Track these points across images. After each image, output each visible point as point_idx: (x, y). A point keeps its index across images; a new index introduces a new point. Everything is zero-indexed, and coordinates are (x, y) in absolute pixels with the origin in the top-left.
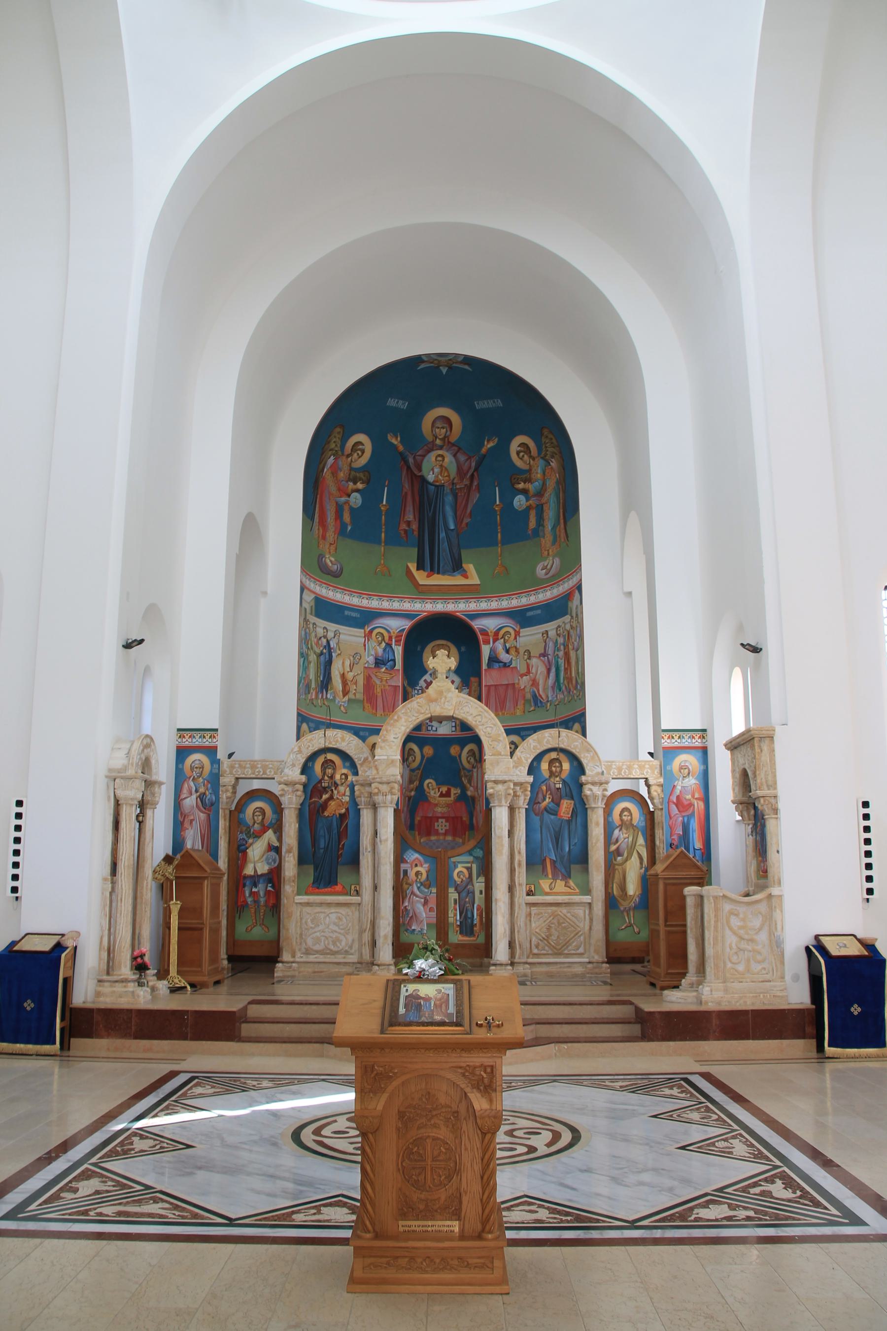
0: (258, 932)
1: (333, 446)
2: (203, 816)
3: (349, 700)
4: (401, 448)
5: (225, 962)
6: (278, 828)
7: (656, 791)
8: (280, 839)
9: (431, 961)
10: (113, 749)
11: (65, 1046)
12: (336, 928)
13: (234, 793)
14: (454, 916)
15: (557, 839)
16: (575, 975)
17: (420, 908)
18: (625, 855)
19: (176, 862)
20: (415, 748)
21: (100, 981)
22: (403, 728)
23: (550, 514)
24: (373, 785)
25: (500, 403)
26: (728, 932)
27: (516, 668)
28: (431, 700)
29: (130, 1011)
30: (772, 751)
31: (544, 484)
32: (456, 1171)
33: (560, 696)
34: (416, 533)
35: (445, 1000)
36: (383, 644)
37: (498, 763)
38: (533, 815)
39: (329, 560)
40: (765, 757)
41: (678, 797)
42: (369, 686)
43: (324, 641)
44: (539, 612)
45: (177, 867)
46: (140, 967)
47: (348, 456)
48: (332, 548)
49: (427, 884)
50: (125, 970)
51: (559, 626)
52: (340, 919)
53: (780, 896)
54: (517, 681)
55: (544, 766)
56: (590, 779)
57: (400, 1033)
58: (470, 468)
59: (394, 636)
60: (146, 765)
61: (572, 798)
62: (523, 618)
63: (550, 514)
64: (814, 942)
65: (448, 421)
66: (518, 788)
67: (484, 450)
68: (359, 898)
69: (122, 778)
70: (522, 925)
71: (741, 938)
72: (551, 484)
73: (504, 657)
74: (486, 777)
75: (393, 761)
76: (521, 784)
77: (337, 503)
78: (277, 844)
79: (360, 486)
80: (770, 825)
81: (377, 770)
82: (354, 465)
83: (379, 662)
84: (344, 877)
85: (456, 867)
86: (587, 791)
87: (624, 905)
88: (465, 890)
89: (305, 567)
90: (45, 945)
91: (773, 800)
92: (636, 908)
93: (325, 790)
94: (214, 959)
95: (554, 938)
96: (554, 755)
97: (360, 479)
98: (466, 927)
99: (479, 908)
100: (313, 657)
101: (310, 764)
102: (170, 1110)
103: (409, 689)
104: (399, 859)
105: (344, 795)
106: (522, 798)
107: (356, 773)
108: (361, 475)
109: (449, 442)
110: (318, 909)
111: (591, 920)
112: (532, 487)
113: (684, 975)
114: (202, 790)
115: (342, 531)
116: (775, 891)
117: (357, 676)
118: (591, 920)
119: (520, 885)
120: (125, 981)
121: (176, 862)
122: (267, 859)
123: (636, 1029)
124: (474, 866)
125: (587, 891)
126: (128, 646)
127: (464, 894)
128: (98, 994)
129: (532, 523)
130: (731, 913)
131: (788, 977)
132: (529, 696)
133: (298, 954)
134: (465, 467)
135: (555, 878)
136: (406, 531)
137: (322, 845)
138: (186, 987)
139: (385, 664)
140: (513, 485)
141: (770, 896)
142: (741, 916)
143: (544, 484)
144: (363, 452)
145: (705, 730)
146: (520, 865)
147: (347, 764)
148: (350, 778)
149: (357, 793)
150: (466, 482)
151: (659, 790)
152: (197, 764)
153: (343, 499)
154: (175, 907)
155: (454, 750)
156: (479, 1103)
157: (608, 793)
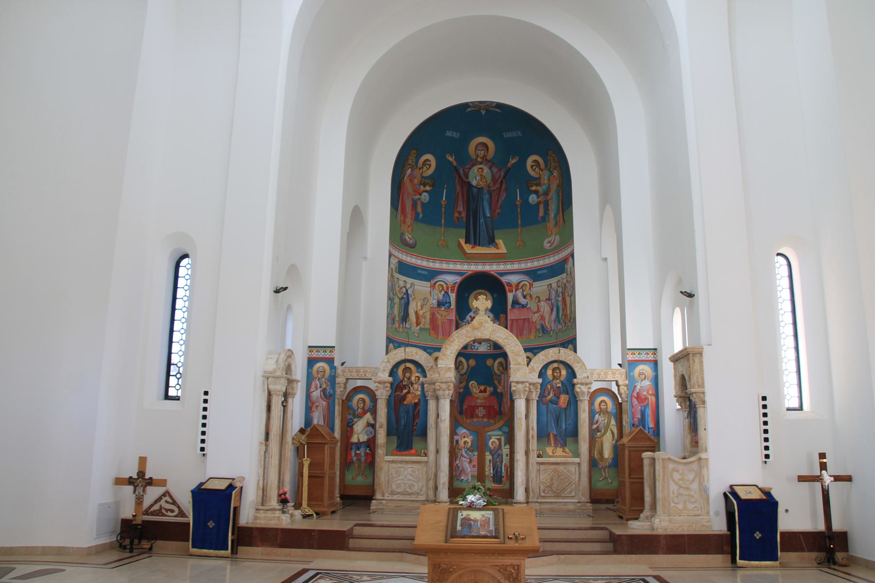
0: (360, 480)
1: (410, 162)
3: (421, 329)
4: (455, 164)
5: (338, 499)
6: (374, 412)
7: (623, 389)
8: (375, 419)
11: (234, 551)
13: (345, 388)
14: (489, 471)
15: (558, 421)
16: (569, 511)
17: (466, 465)
21: (257, 510)
25: (520, 134)
26: (672, 483)
28: (475, 329)
29: (277, 529)
30: (701, 362)
31: (549, 187)
34: (465, 219)
39: (408, 237)
40: (696, 366)
42: (433, 319)
43: (404, 289)
45: (308, 436)
46: (284, 501)
49: (471, 450)
50: (274, 503)
52: (414, 472)
55: (549, 372)
56: (579, 381)
57: (457, 542)
60: (288, 369)
61: (568, 394)
62: (535, 275)
63: (553, 207)
64: (729, 490)
67: (509, 165)
71: (681, 487)
72: (554, 187)
73: (522, 301)
74: (511, 379)
75: (449, 368)
76: (534, 384)
79: (428, 188)
80: (700, 412)
83: (440, 304)
84: (417, 445)
85: (490, 438)
86: (577, 389)
87: (602, 464)
88: (496, 453)
89: (392, 242)
90: (222, 485)
91: (701, 395)
92: (609, 466)
93: (405, 387)
95: (555, 486)
96: (555, 365)
98: (497, 478)
100: (397, 300)
103: (460, 322)
104: (453, 433)
106: (534, 393)
107: (425, 376)
108: (429, 181)
110: (400, 465)
111: (580, 474)
112: (540, 189)
113: (642, 511)
114: (324, 386)
115: (416, 218)
117: (426, 313)
118: (580, 474)
123: (610, 546)
124: (503, 438)
125: (577, 454)
127: (496, 456)
128: (256, 518)
129: (541, 213)
130: (674, 470)
131: (712, 513)
132: (538, 327)
133: (386, 495)
134: (497, 177)
135: (556, 446)
136: (458, 218)
137: (403, 423)
140: (528, 188)
141: (700, 459)
143: (549, 187)
144: (430, 166)
148: (421, 379)
149: (426, 389)
150: (498, 186)
151: (625, 388)
154: (306, 462)
155: (489, 362)
157: (592, 391)
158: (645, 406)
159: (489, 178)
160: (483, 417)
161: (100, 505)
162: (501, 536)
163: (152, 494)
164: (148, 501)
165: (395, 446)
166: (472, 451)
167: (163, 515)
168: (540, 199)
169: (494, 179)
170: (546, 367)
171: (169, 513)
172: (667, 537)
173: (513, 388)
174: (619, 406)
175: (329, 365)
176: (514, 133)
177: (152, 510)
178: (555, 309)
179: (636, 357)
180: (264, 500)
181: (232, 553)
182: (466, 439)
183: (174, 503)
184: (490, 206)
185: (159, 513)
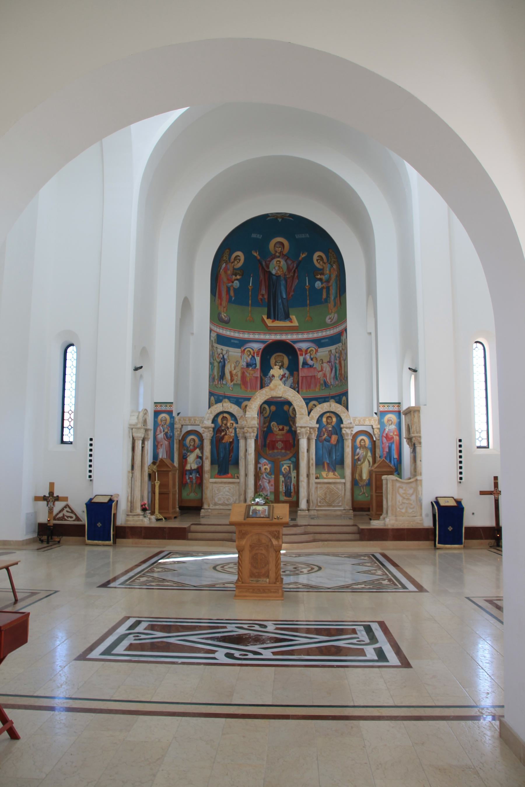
0: (192, 496)
1: (225, 258)
2: (167, 443)
3: (234, 384)
4: (259, 257)
5: (178, 509)
6: (201, 448)
7: (376, 431)
8: (202, 453)
9: (261, 499)
10: (131, 416)
11: (115, 542)
12: (228, 494)
13: (181, 432)
15: (330, 454)
16: (337, 516)
18: (362, 460)
19: (157, 464)
20: (267, 407)
21: (128, 515)
22: (259, 403)
23: (333, 291)
24: (245, 429)
25: (308, 236)
26: (398, 495)
27: (316, 368)
28: (271, 390)
29: (141, 527)
30: (419, 417)
31: (330, 276)
32: (268, 563)
33: (337, 383)
34: (266, 300)
35: (265, 510)
36: (250, 356)
37: (302, 419)
38: (319, 442)
39: (223, 315)
40: (416, 420)
41: (387, 434)
42: (243, 377)
43: (221, 355)
44: (327, 340)
45: (158, 467)
46: (144, 510)
47: (232, 263)
48: (225, 309)
49: (270, 474)
50: (139, 511)
51: (337, 348)
52: (230, 489)
53: (421, 480)
54: (316, 375)
55: (324, 419)
56: (345, 426)
57: (250, 520)
58: (293, 267)
59: (256, 352)
60: (145, 422)
61: (337, 434)
62: (319, 343)
63: (333, 291)
64: (435, 500)
65: (282, 244)
66: (312, 430)
67: (300, 259)
68: (238, 480)
69: (135, 428)
70: (313, 492)
71: (404, 498)
72: (333, 277)
73: (310, 362)
74: (297, 425)
75: (254, 418)
76: (313, 428)
77: (227, 287)
78: (200, 455)
79: (238, 277)
80: (418, 449)
81: (247, 421)
82: (235, 267)
83: (248, 365)
84: (232, 470)
85: (283, 466)
86: (343, 432)
87: (361, 484)
88: (287, 476)
89: (212, 320)
90: (105, 500)
91: (419, 439)
92: (367, 485)
93: (223, 431)
94: (174, 508)
95: (328, 498)
96: (328, 414)
97: (238, 274)
98: (288, 493)
99: (294, 485)
100: (216, 364)
101: (216, 419)
102: (169, 558)
103: (263, 377)
104: (257, 462)
105: (232, 433)
106: (313, 434)
107: (237, 423)
108: (238, 272)
109: (283, 254)
110: (220, 485)
111: (345, 490)
112: (324, 278)
113: (381, 515)
114: (166, 431)
115: (230, 301)
116: (419, 478)
118: (345, 490)
119: (312, 474)
120: (138, 515)
121: (157, 464)
122: (196, 462)
123: (357, 536)
124: (292, 466)
125: (343, 477)
126: (136, 369)
127: (287, 478)
128: (127, 521)
129: (324, 296)
130: (400, 487)
131: (423, 515)
132: (322, 382)
133: (211, 505)
134: (291, 267)
135: (329, 471)
136: (261, 299)
137: (222, 455)
138: (162, 519)
139: (251, 366)
140: (315, 276)
141: (417, 480)
142: (404, 488)
143: (330, 276)
144: (240, 260)
145: (399, 403)
146: (312, 465)
147: (233, 419)
148: (234, 425)
149: (237, 432)
150: (292, 274)
151: (378, 431)
152: (164, 419)
153: (230, 284)
154: (157, 484)
156: (275, 542)
157: (354, 433)
158: (392, 443)
159: (285, 268)
160: (282, 449)
161: (27, 514)
162: (271, 517)
163: (59, 506)
164: (56, 510)
165: (217, 471)
166: (270, 475)
167: (66, 520)
168: (324, 285)
169: (289, 269)
170: (322, 416)
171: (69, 519)
172: (393, 530)
173: (298, 431)
174: (374, 443)
175: (169, 415)
176: (303, 235)
177: (58, 517)
178: (334, 369)
179: (386, 409)
180: (132, 508)
181: (113, 543)
182: (266, 467)
183: (72, 512)
184: (286, 290)
185: (63, 518)
